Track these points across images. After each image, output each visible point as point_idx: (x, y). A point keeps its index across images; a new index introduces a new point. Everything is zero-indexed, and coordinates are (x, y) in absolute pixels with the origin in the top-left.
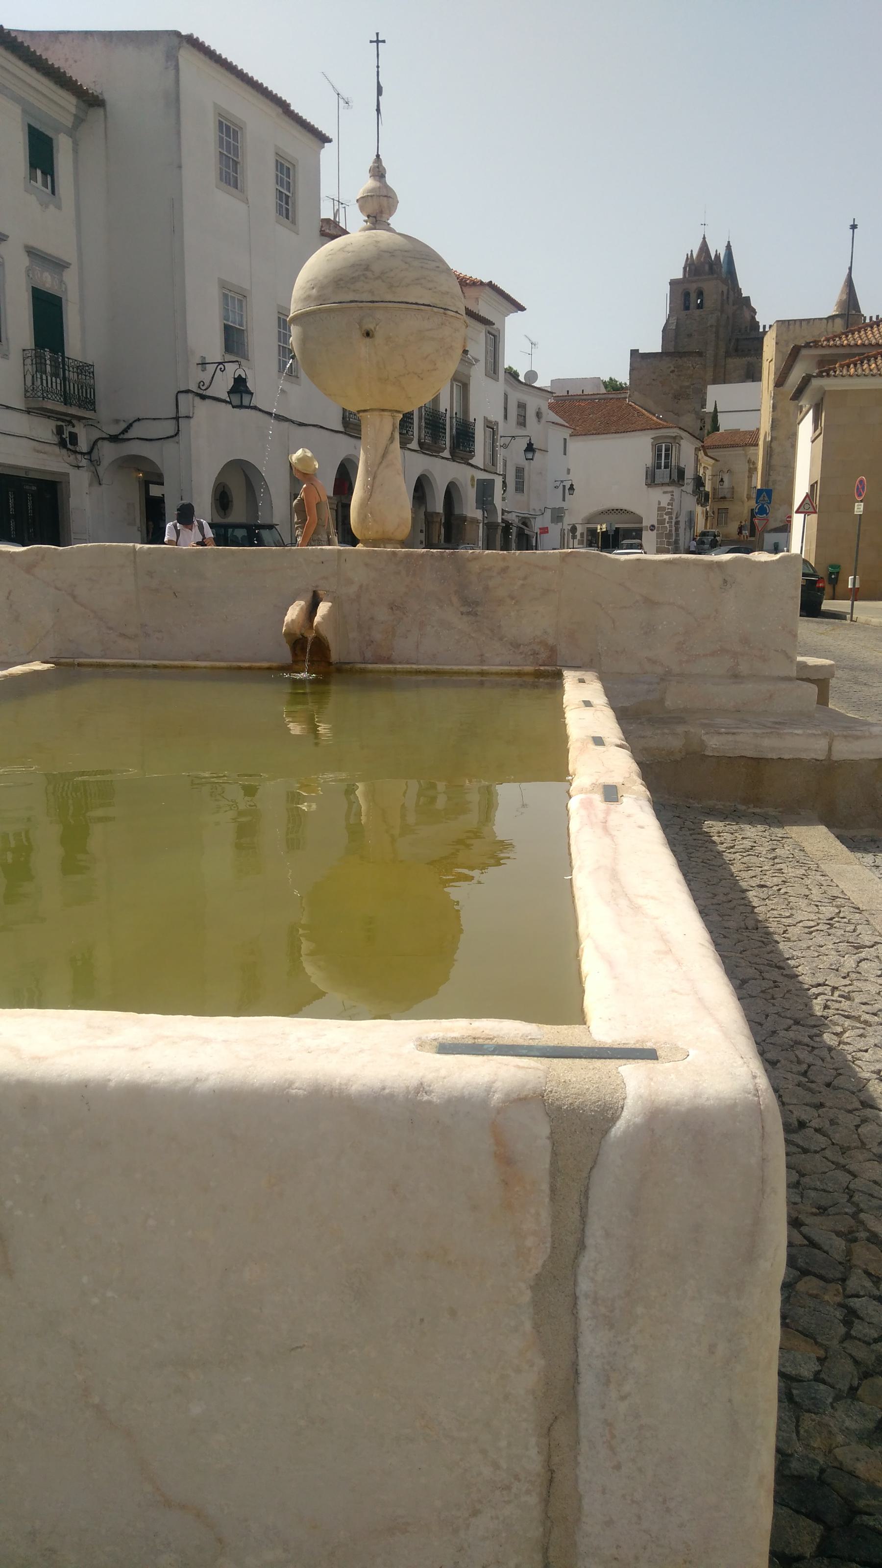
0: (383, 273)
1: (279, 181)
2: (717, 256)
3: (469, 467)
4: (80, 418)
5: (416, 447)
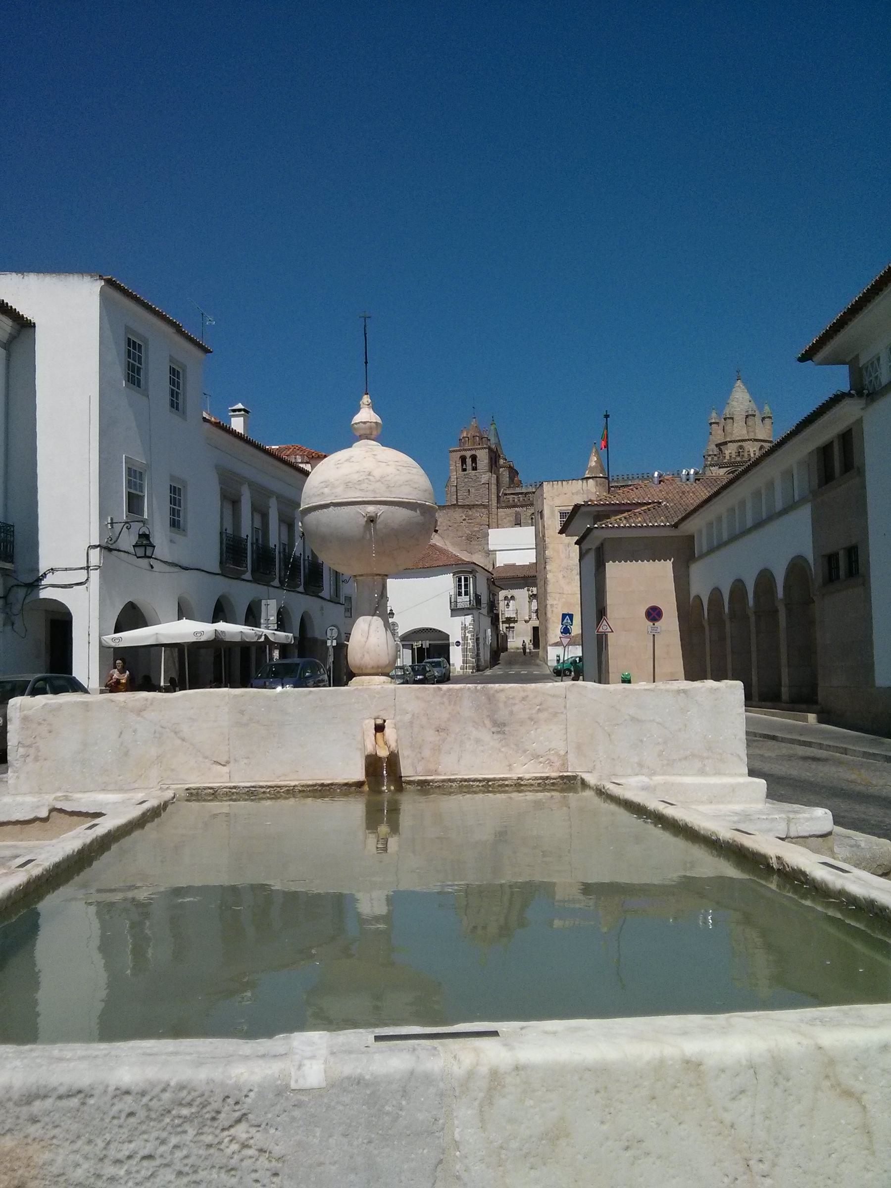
0: (382, 477)
1: (172, 382)
2: (698, 597)
3: (320, 600)
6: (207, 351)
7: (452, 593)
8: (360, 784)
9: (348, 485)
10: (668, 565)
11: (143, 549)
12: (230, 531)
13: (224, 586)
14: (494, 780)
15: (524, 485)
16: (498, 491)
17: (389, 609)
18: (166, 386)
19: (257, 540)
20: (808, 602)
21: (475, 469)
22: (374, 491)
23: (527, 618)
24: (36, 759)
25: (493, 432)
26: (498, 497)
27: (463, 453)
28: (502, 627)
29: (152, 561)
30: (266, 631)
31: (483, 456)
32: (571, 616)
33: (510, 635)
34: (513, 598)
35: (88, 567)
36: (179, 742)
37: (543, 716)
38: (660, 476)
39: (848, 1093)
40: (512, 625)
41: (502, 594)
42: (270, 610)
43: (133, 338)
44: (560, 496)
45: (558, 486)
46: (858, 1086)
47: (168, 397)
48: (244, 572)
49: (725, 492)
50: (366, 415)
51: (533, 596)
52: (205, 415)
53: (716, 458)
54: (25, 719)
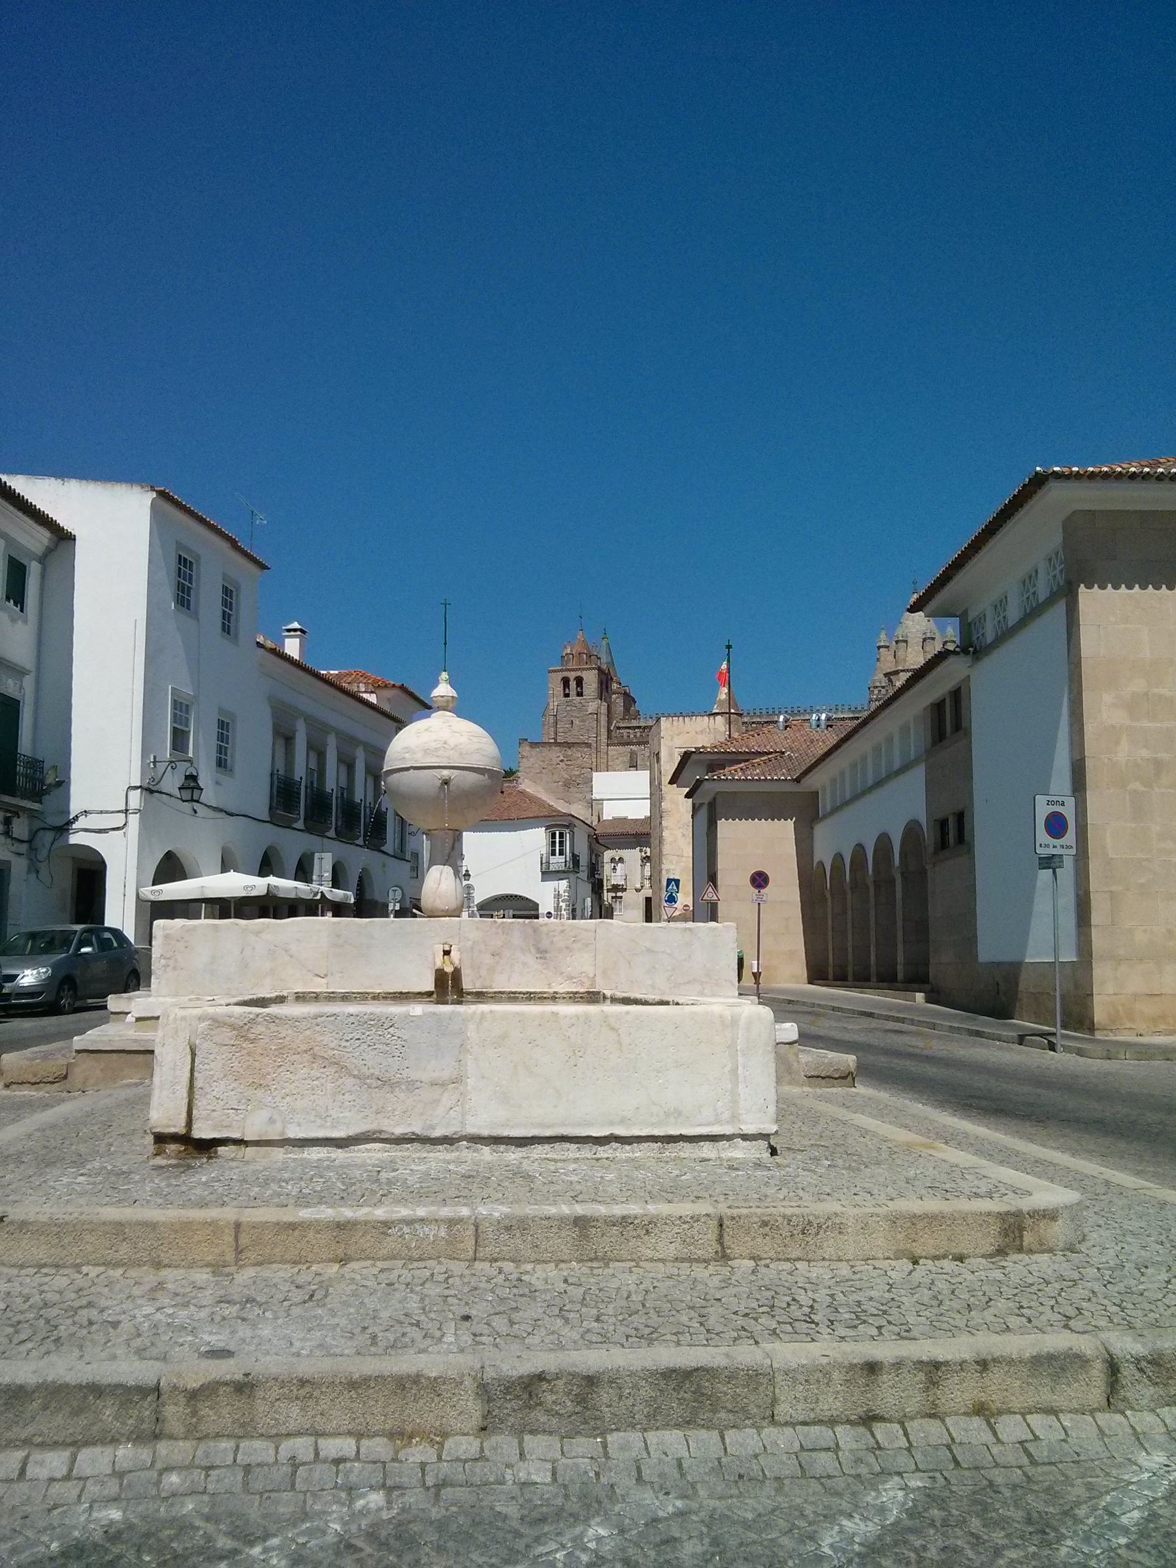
1: (225, 603)
2: (821, 863)
3: (380, 855)
4: (24, 809)
5: (334, 836)
6: (263, 567)
7: (544, 851)
8: (430, 994)
9: (426, 752)
10: (789, 825)
11: (189, 791)
12: (281, 772)
13: (272, 835)
14: (535, 993)
15: (642, 716)
16: (609, 723)
17: (464, 869)
18: (218, 608)
19: (312, 783)
20: (923, 873)
21: (580, 694)
22: (448, 758)
23: (638, 886)
24: (175, 968)
25: (604, 649)
26: (609, 731)
27: (566, 674)
28: (607, 897)
29: (196, 806)
30: (322, 888)
31: (591, 679)
32: (677, 882)
33: (617, 906)
34: (621, 860)
35: (127, 810)
36: (287, 958)
37: (575, 946)
38: (786, 720)
39: (613, 1029)
40: (619, 894)
41: (608, 855)
42: (324, 864)
43: (184, 555)
44: (681, 735)
45: (678, 722)
46: (617, 1026)
47: (218, 621)
48: (297, 820)
49: (845, 746)
50: (443, 690)
51: (647, 859)
52: (260, 639)
53: (883, 691)
54: (167, 937)
